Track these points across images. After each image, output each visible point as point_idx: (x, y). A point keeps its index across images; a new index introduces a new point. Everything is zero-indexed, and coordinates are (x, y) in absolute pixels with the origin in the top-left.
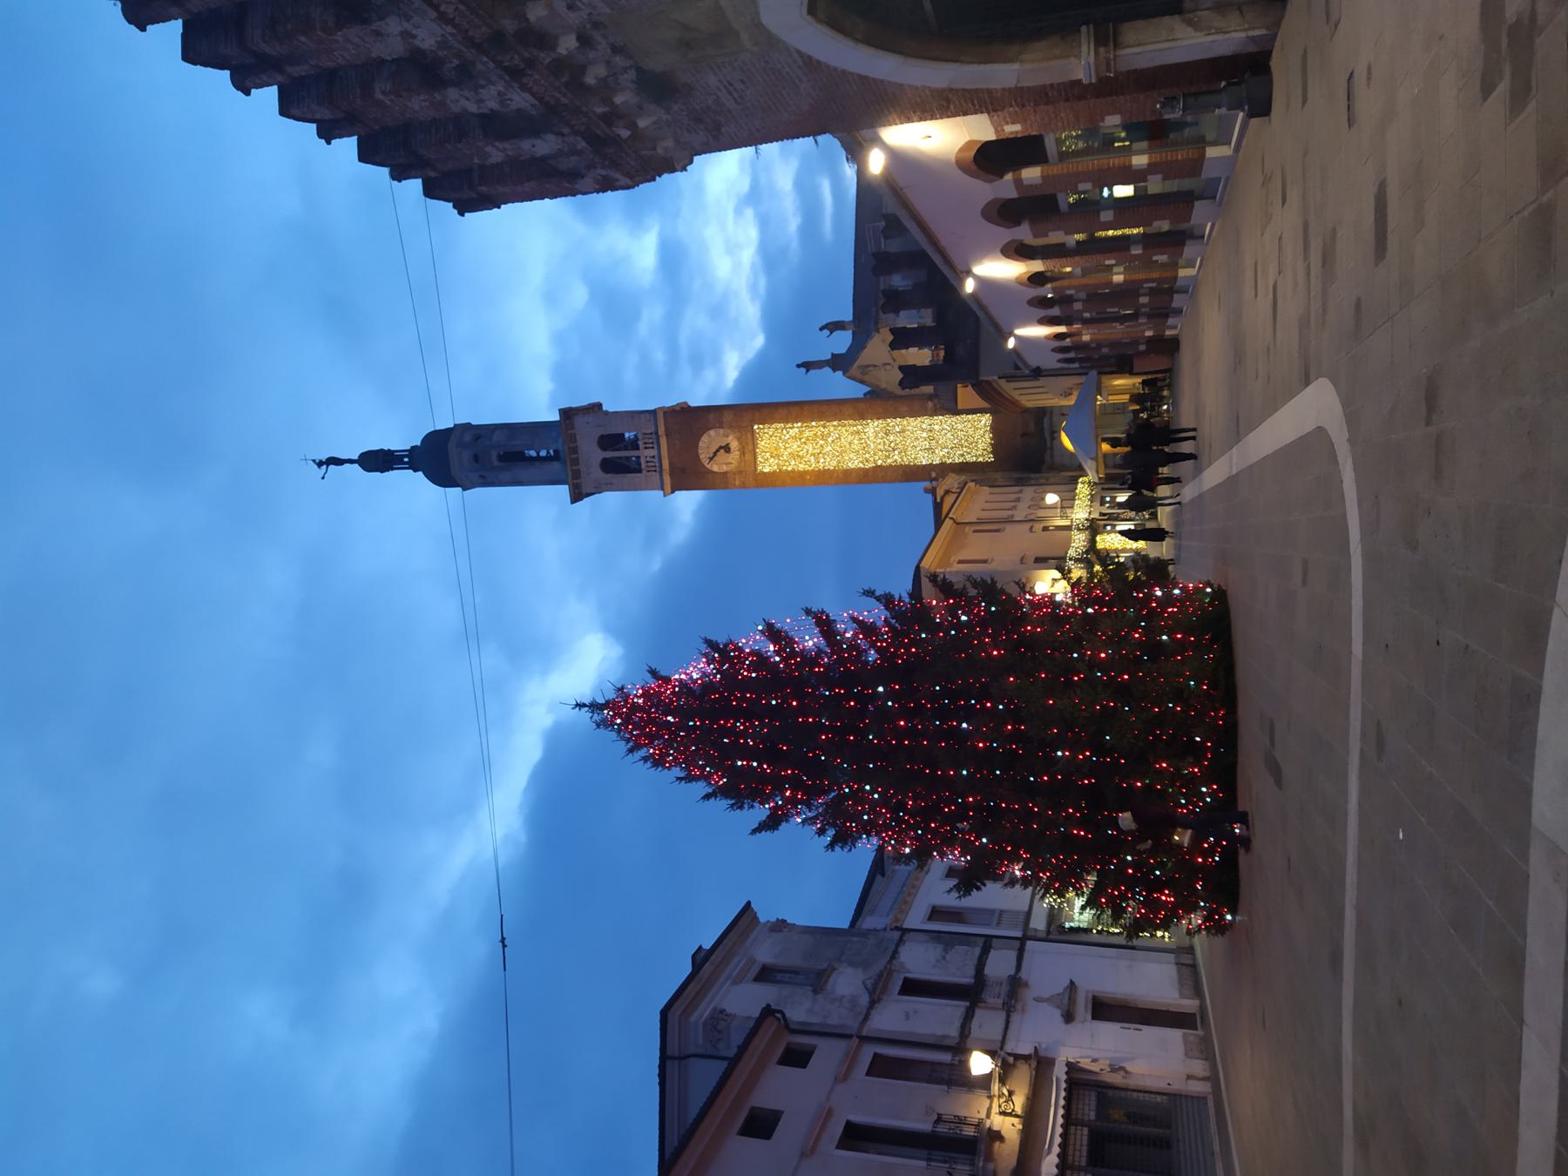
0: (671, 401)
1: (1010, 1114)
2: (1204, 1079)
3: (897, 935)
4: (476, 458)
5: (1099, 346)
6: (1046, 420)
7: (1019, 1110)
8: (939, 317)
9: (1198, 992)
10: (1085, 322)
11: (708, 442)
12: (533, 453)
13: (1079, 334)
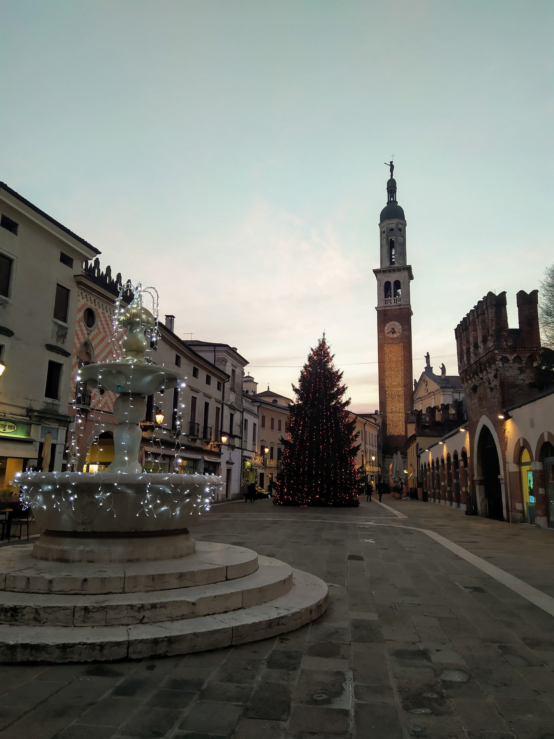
0: (413, 309)
4: (392, 230)
5: (426, 477)
7: (213, 449)
8: (438, 423)
9: (233, 499)
10: (433, 473)
11: (397, 326)
12: (393, 253)
13: (429, 471)
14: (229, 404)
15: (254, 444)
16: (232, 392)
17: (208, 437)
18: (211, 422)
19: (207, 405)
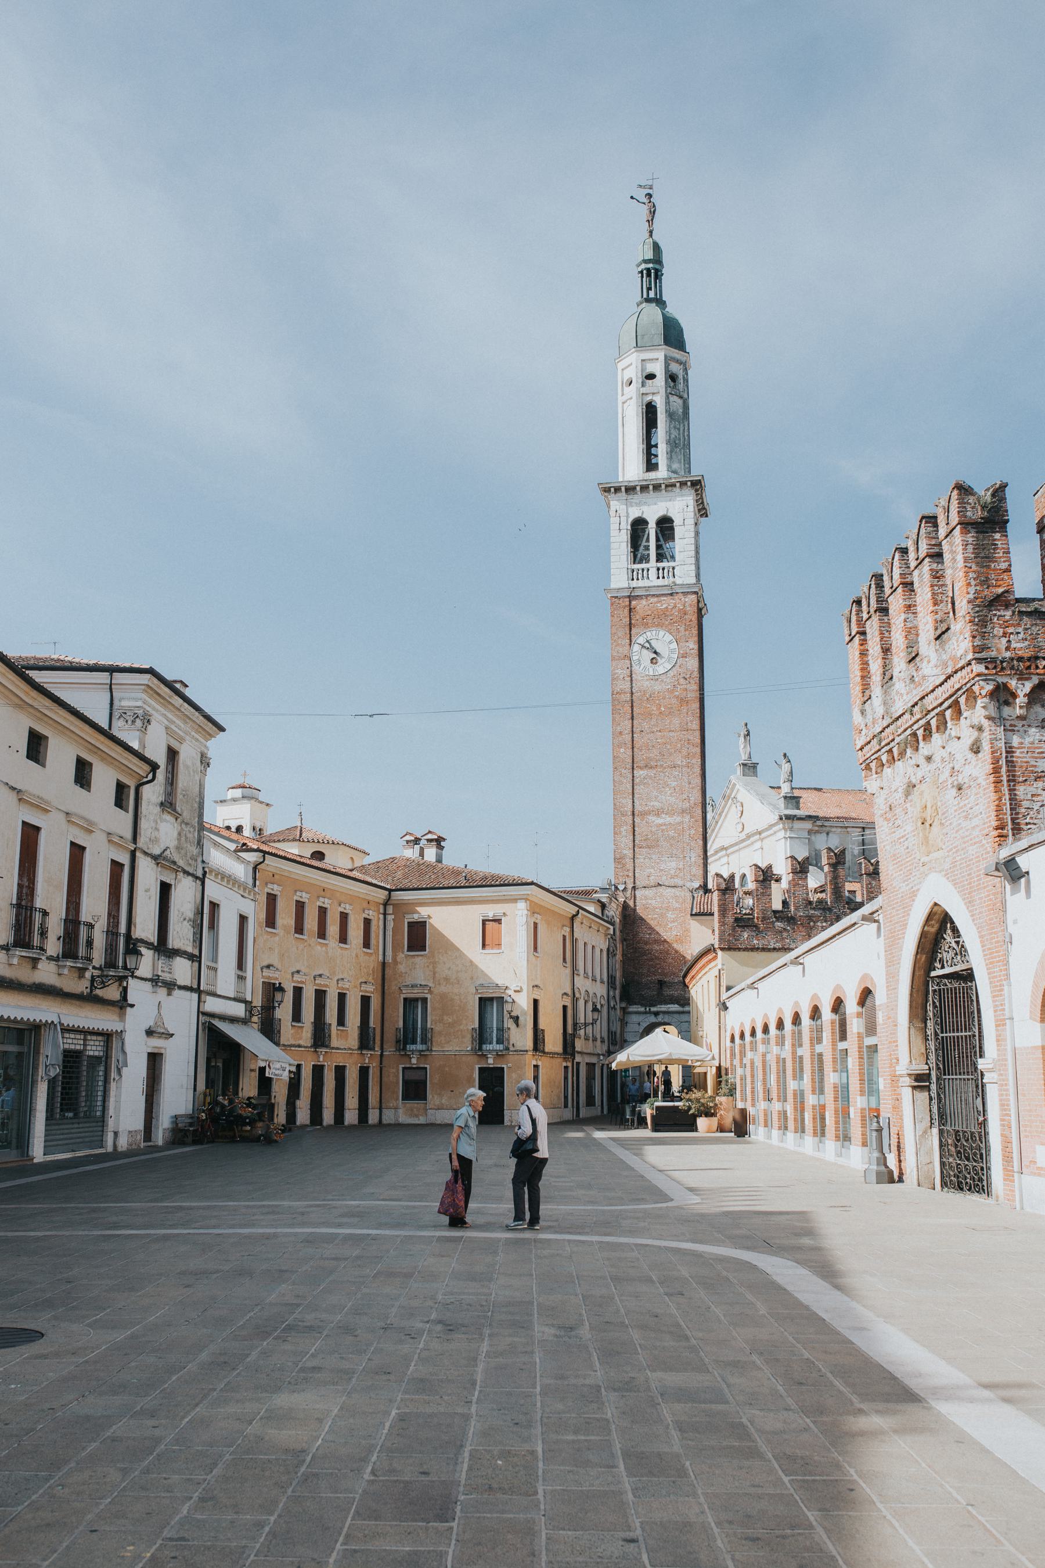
1: (92, 985)
2: (115, 1146)
3: (200, 874)
6: (674, 1007)
14: (157, 851)
15: (241, 978)
16: (167, 817)
17: (82, 951)
18: (94, 905)
19: (77, 851)
